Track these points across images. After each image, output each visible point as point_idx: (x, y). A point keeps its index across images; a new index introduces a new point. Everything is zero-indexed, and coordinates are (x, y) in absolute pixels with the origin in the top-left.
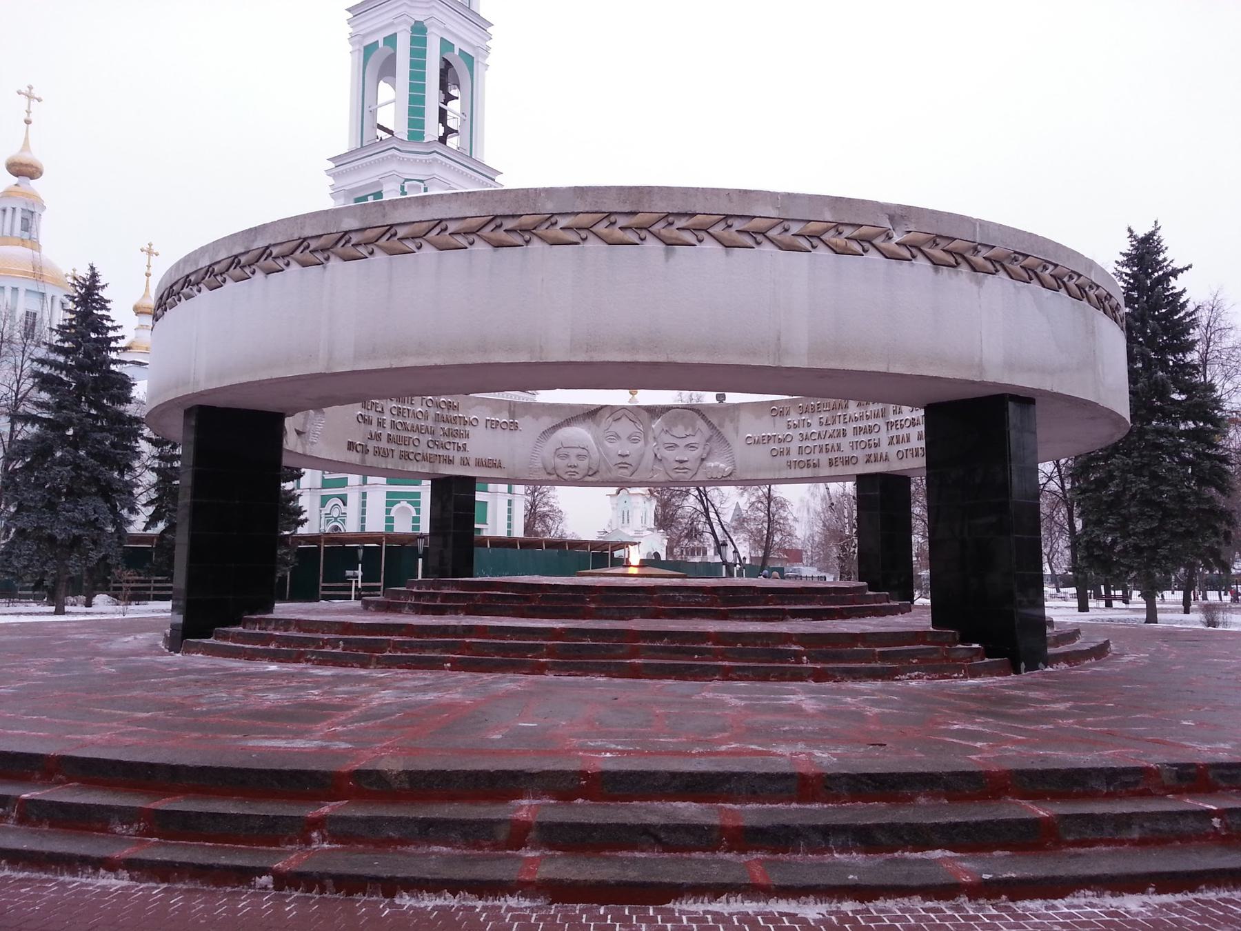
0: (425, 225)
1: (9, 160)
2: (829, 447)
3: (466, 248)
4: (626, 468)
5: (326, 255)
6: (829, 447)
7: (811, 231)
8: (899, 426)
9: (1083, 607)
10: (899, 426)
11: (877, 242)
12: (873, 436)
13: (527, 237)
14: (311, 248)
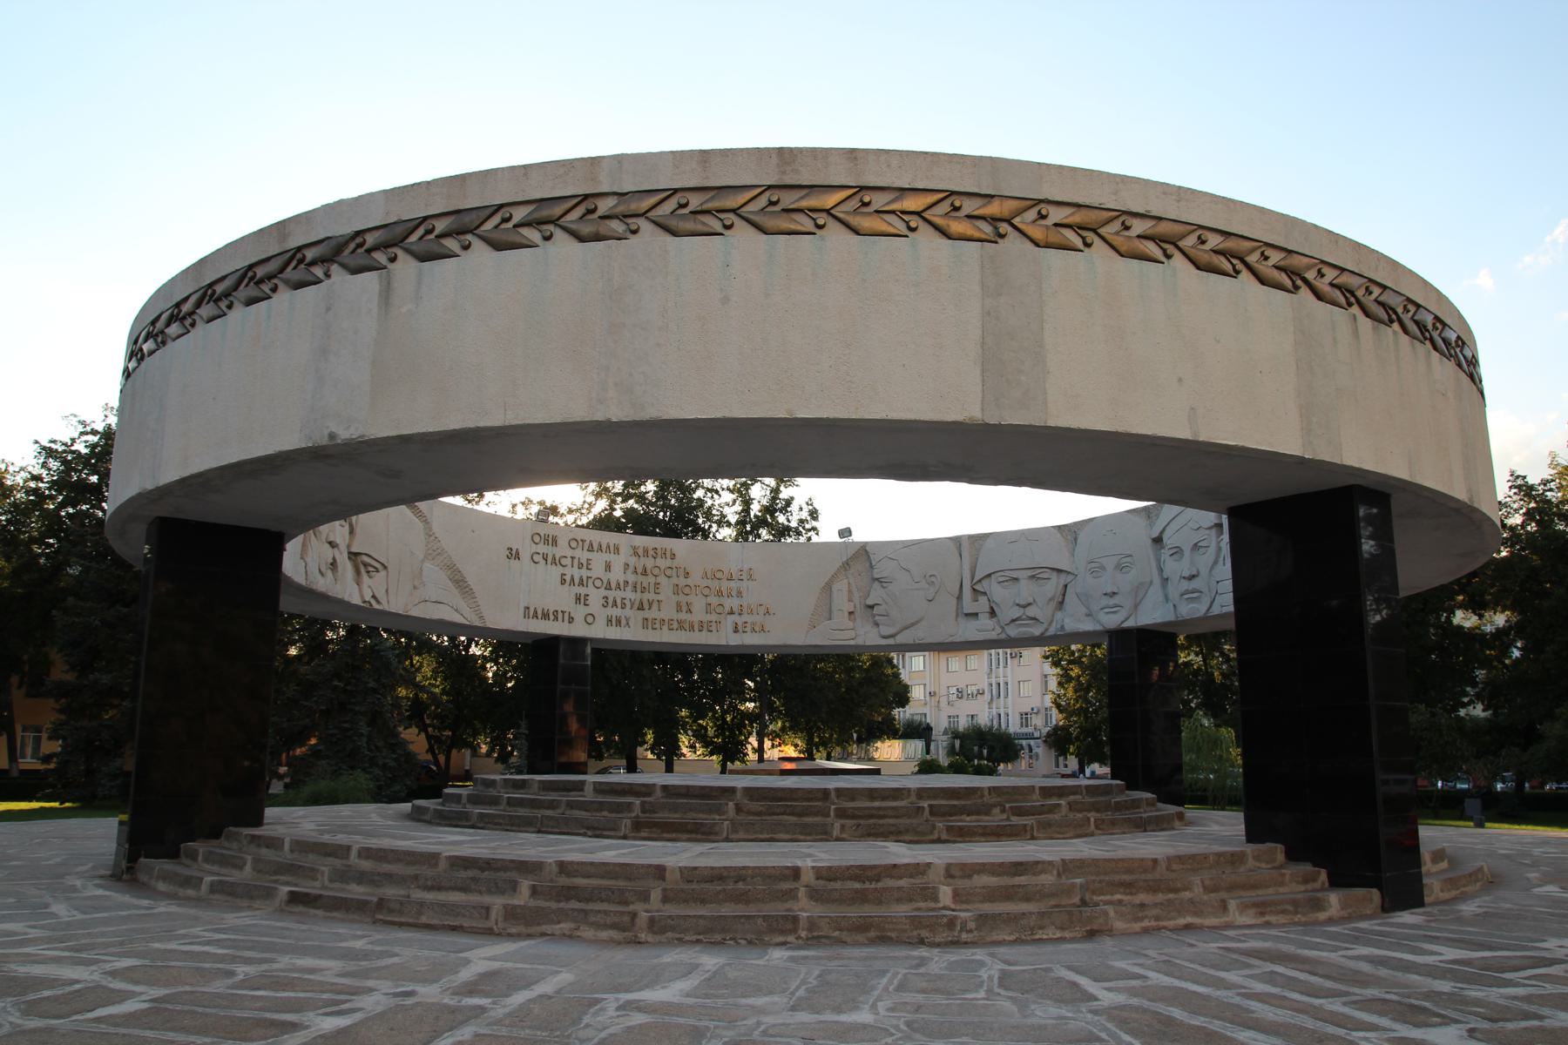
8: (657, 626)
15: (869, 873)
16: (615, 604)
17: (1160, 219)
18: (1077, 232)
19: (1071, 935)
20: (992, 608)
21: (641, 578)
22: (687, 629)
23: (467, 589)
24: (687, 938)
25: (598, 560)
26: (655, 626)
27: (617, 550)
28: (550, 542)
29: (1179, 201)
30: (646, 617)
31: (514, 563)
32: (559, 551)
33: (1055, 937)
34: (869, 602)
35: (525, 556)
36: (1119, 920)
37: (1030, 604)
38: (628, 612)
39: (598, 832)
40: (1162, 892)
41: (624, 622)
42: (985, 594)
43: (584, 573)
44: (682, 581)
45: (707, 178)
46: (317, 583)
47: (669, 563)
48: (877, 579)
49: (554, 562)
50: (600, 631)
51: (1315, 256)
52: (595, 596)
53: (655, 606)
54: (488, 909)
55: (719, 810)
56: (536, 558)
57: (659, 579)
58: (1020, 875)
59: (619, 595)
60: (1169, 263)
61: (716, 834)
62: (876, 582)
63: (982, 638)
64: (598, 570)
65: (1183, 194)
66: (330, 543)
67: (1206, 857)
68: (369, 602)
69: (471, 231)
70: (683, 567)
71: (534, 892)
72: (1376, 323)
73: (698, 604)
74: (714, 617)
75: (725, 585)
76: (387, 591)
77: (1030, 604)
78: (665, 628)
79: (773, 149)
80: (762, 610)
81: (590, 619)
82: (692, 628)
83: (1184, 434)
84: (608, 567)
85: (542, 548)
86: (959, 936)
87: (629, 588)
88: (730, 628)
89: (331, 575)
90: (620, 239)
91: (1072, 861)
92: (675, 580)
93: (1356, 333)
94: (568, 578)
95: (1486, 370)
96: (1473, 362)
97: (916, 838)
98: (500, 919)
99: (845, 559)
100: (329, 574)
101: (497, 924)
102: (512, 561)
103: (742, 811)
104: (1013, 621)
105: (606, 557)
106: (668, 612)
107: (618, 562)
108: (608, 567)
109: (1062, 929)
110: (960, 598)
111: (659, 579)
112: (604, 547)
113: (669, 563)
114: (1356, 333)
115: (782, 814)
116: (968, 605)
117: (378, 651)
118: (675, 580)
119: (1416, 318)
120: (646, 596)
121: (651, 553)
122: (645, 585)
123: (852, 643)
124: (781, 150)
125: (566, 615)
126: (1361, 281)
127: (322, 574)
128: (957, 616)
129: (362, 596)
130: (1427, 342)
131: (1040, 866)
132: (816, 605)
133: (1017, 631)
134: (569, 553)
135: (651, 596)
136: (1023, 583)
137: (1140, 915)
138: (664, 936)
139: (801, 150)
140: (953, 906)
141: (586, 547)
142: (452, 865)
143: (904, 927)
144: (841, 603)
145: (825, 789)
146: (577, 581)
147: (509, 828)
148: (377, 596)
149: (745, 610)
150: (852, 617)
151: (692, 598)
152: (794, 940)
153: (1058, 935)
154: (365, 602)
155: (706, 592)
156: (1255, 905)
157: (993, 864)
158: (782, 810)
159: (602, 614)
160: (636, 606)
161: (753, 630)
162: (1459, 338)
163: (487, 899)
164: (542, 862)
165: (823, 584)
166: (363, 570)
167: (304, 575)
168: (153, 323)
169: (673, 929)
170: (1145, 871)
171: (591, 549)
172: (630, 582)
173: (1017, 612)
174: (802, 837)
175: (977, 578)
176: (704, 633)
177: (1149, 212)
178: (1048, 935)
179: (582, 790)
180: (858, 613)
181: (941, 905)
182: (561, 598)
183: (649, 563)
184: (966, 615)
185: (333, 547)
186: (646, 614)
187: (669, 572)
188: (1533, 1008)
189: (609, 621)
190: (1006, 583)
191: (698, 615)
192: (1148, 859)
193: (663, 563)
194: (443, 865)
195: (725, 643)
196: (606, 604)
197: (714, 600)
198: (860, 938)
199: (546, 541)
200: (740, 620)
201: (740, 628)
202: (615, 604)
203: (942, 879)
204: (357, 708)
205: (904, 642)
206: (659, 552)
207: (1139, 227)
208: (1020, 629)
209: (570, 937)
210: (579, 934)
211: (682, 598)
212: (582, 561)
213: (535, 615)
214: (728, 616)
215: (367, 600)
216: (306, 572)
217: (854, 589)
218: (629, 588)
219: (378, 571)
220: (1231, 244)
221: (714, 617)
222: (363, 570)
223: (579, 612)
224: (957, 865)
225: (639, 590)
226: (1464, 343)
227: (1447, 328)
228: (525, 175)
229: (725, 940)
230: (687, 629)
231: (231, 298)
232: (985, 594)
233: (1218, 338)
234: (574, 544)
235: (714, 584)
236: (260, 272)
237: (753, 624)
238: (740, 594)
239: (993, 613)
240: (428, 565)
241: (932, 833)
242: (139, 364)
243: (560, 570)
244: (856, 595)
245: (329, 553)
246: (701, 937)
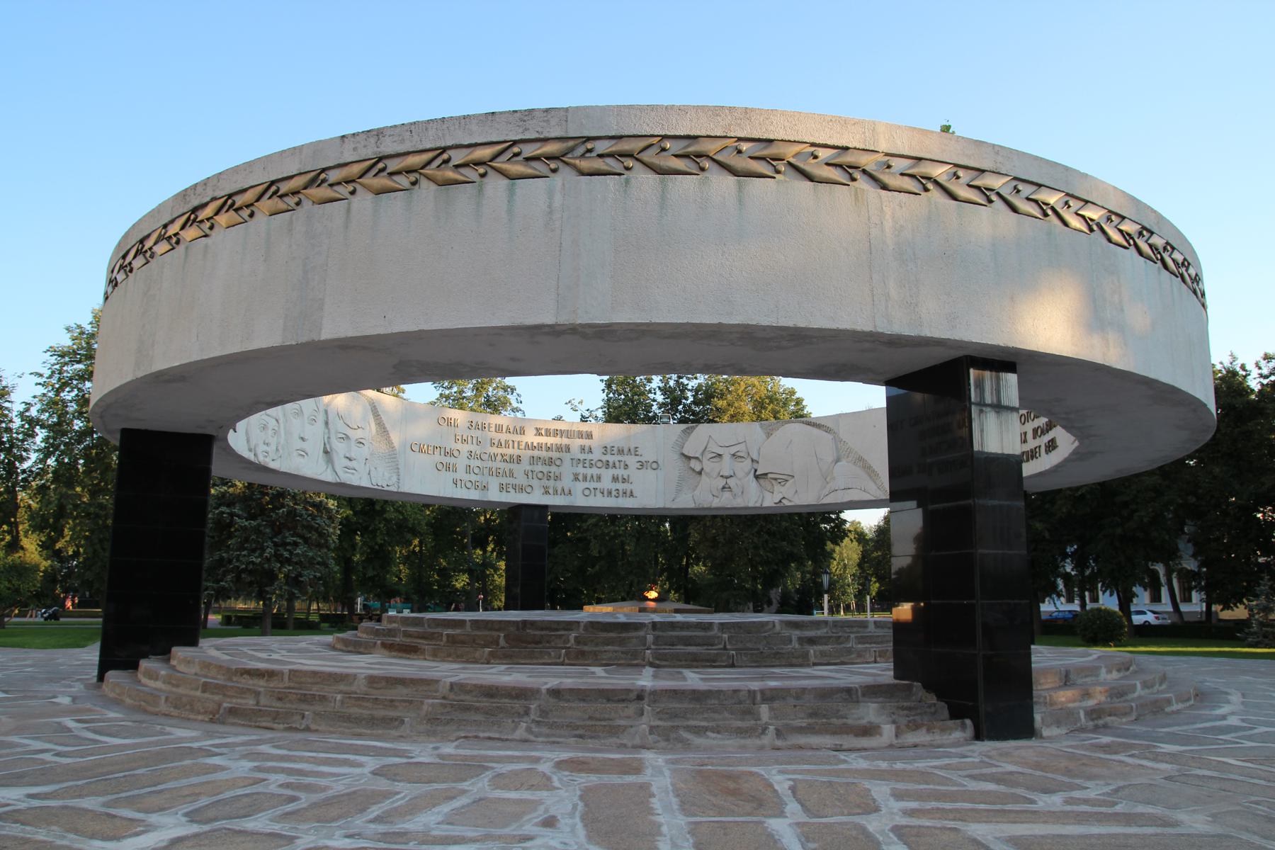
2: (501, 471)
3: (620, 174)
4: (353, 474)
6: (501, 471)
7: (849, 162)
8: (587, 465)
10: (587, 465)
12: (553, 469)
13: (481, 170)
37: (731, 476)
77: (731, 476)
78: (581, 465)
95: (1208, 285)
96: (1197, 279)
119: (1149, 242)
126: (1103, 212)
130: (1159, 262)
138: (312, 708)
162: (1185, 259)
164: (711, 623)
168: (124, 257)
188: (289, 792)
226: (1189, 264)
227: (1175, 251)
231: (301, 196)
236: (284, 188)
242: (114, 289)
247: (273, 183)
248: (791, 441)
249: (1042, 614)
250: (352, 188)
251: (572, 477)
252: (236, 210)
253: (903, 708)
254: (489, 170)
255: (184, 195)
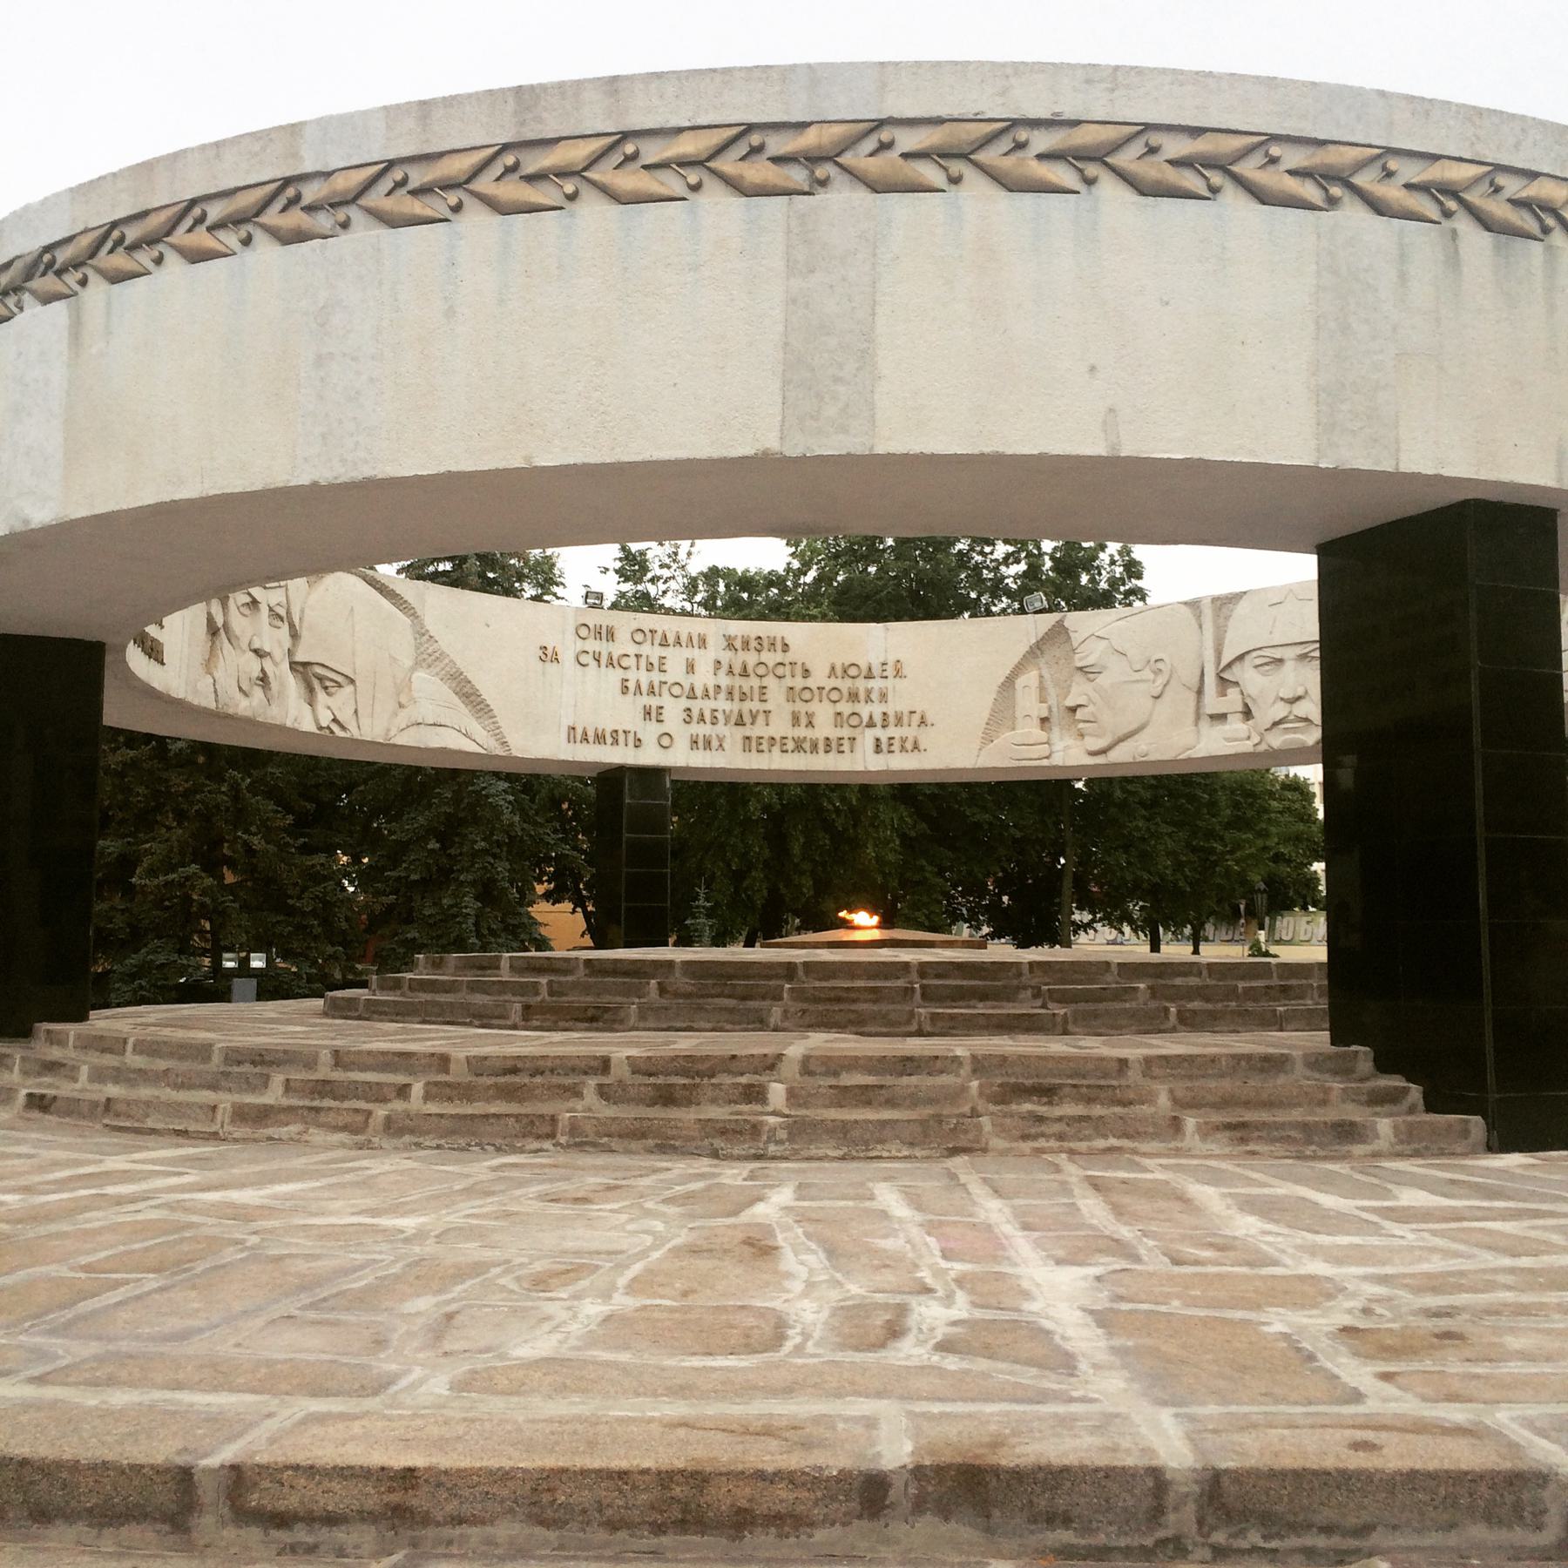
0: (260, 193)
1: (801, 134)
5: (243, 234)
8: (764, 747)
9: (1155, 947)
11: (1361, 180)
14: (209, 222)
15: (700, 1067)
16: (702, 719)
17: (1076, 123)
18: (937, 162)
19: (924, 1153)
20: (1246, 705)
21: (738, 681)
22: (808, 749)
23: (482, 706)
24: (427, 1143)
25: (676, 659)
26: (761, 748)
27: (703, 643)
28: (604, 635)
29: (1113, 90)
30: (748, 734)
31: (552, 668)
32: (617, 649)
33: (900, 1155)
34: (1070, 702)
35: (567, 657)
36: (998, 1136)
38: (721, 728)
39: (485, 1021)
40: (1103, 1104)
41: (715, 743)
42: (1237, 684)
43: (656, 677)
44: (799, 683)
45: (427, 141)
46: (237, 705)
47: (779, 657)
48: (1081, 669)
49: (610, 663)
50: (681, 757)
51: (1374, 143)
52: (674, 710)
53: (761, 719)
54: (214, 1108)
55: (628, 992)
56: (583, 659)
57: (765, 682)
58: (910, 1075)
59: (708, 705)
60: (1090, 193)
61: (622, 1022)
62: (1079, 673)
63: (1232, 751)
64: (675, 672)
65: (1117, 77)
66: (256, 651)
67: (1214, 1060)
68: (328, 728)
69: (964, 157)
70: (799, 663)
71: (288, 1086)
72: (1503, 238)
73: (823, 712)
74: (846, 732)
75: (861, 685)
76: (356, 712)
78: (776, 749)
79: (509, 89)
80: (916, 719)
81: (666, 741)
82: (814, 747)
83: (1094, 447)
84: (691, 667)
85: (592, 645)
86: (766, 1149)
87: (722, 695)
88: (869, 744)
89: (262, 696)
90: (325, 237)
91: (985, 1057)
92: (788, 682)
93: (1453, 261)
94: (631, 685)
97: (884, 1030)
98: (227, 1120)
99: (1034, 641)
100: (258, 693)
101: (222, 1126)
102: (548, 664)
103: (668, 992)
104: (1275, 724)
105: (687, 653)
106: (780, 726)
107: (704, 659)
108: (691, 667)
109: (912, 1144)
110: (1200, 692)
111: (765, 682)
112: (684, 639)
113: (779, 657)
114: (1453, 261)
115: (718, 996)
116: (1212, 703)
117: (487, 796)
118: (788, 682)
120: (748, 706)
121: (753, 644)
122: (746, 689)
123: (1045, 763)
124: (519, 90)
125: (631, 738)
127: (246, 694)
128: (1198, 717)
129: (317, 721)
131: (939, 1064)
132: (993, 710)
133: (1282, 738)
134: (632, 649)
135: (755, 705)
136: (1289, 666)
137: (1033, 1131)
139: (544, 88)
140: (787, 1112)
141: (657, 641)
142: (226, 1059)
143: (692, 1133)
144: (1028, 703)
145: (790, 963)
146: (644, 688)
147: (394, 1018)
148: (339, 717)
149: (892, 719)
150: (1047, 725)
151: (814, 707)
152: (552, 1148)
153: (906, 1153)
154: (320, 728)
155: (835, 696)
156: (1229, 1127)
157: (870, 1058)
158: (719, 990)
159: (682, 734)
160: (733, 720)
161: (903, 749)
163: (432, 1108)
165: (1002, 680)
166: (316, 684)
167: (213, 695)
169: (412, 1132)
170: (1105, 1076)
171: (664, 643)
172: (723, 687)
173: (1280, 711)
174: (729, 1027)
175: (1224, 662)
176: (832, 755)
177: (1057, 114)
178: (889, 1151)
179: (498, 968)
180: (1054, 720)
181: (770, 1109)
182: (626, 714)
183: (751, 658)
184: (1212, 717)
185: (261, 656)
186: (748, 731)
187: (780, 670)
189: (694, 742)
190: (1267, 668)
191: (824, 728)
192: (1111, 1059)
193: (770, 658)
194: (216, 1058)
195: (862, 769)
196: (688, 719)
197: (845, 708)
198: (634, 1145)
199: (598, 634)
200: (883, 735)
201: (884, 746)
202: (702, 719)
203: (798, 1076)
204: (462, 878)
205: (1120, 760)
206: (765, 643)
207: (1042, 141)
208: (1287, 736)
209: (298, 1141)
210: (308, 1138)
211: (801, 708)
212: (651, 660)
213: (585, 739)
214: (867, 730)
215: (324, 725)
216: (216, 691)
217: (1049, 684)
218: (722, 695)
219: (340, 686)
220: (1202, 146)
221: (846, 732)
222: (316, 684)
223: (650, 731)
224: (817, 1058)
225: (737, 696)
228: (218, 156)
229: (470, 1145)
230: (808, 749)
232: (1237, 684)
233: (1165, 299)
234: (639, 637)
235: (845, 685)
236: (62, 256)
237: (903, 740)
238: (883, 697)
239: (1247, 714)
240: (421, 675)
241: (909, 1022)
243: (620, 673)
244: (1052, 692)
245: (253, 666)
246: (442, 1142)
247: (193, 202)
248: (352, 609)
249: (1327, 1025)
250: (157, 254)
251: (687, 743)
252: (59, 273)
253: (1219, 1128)
254: (466, 199)
255: (525, 97)
